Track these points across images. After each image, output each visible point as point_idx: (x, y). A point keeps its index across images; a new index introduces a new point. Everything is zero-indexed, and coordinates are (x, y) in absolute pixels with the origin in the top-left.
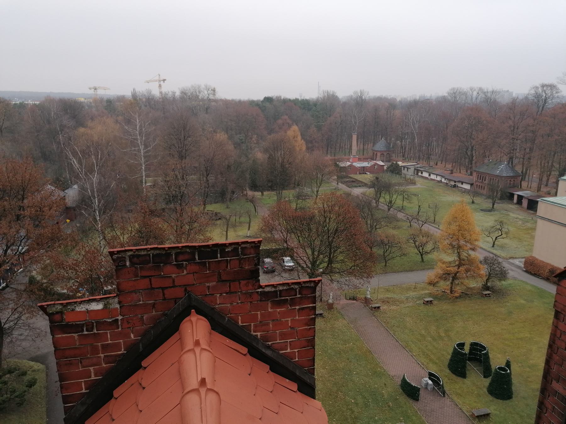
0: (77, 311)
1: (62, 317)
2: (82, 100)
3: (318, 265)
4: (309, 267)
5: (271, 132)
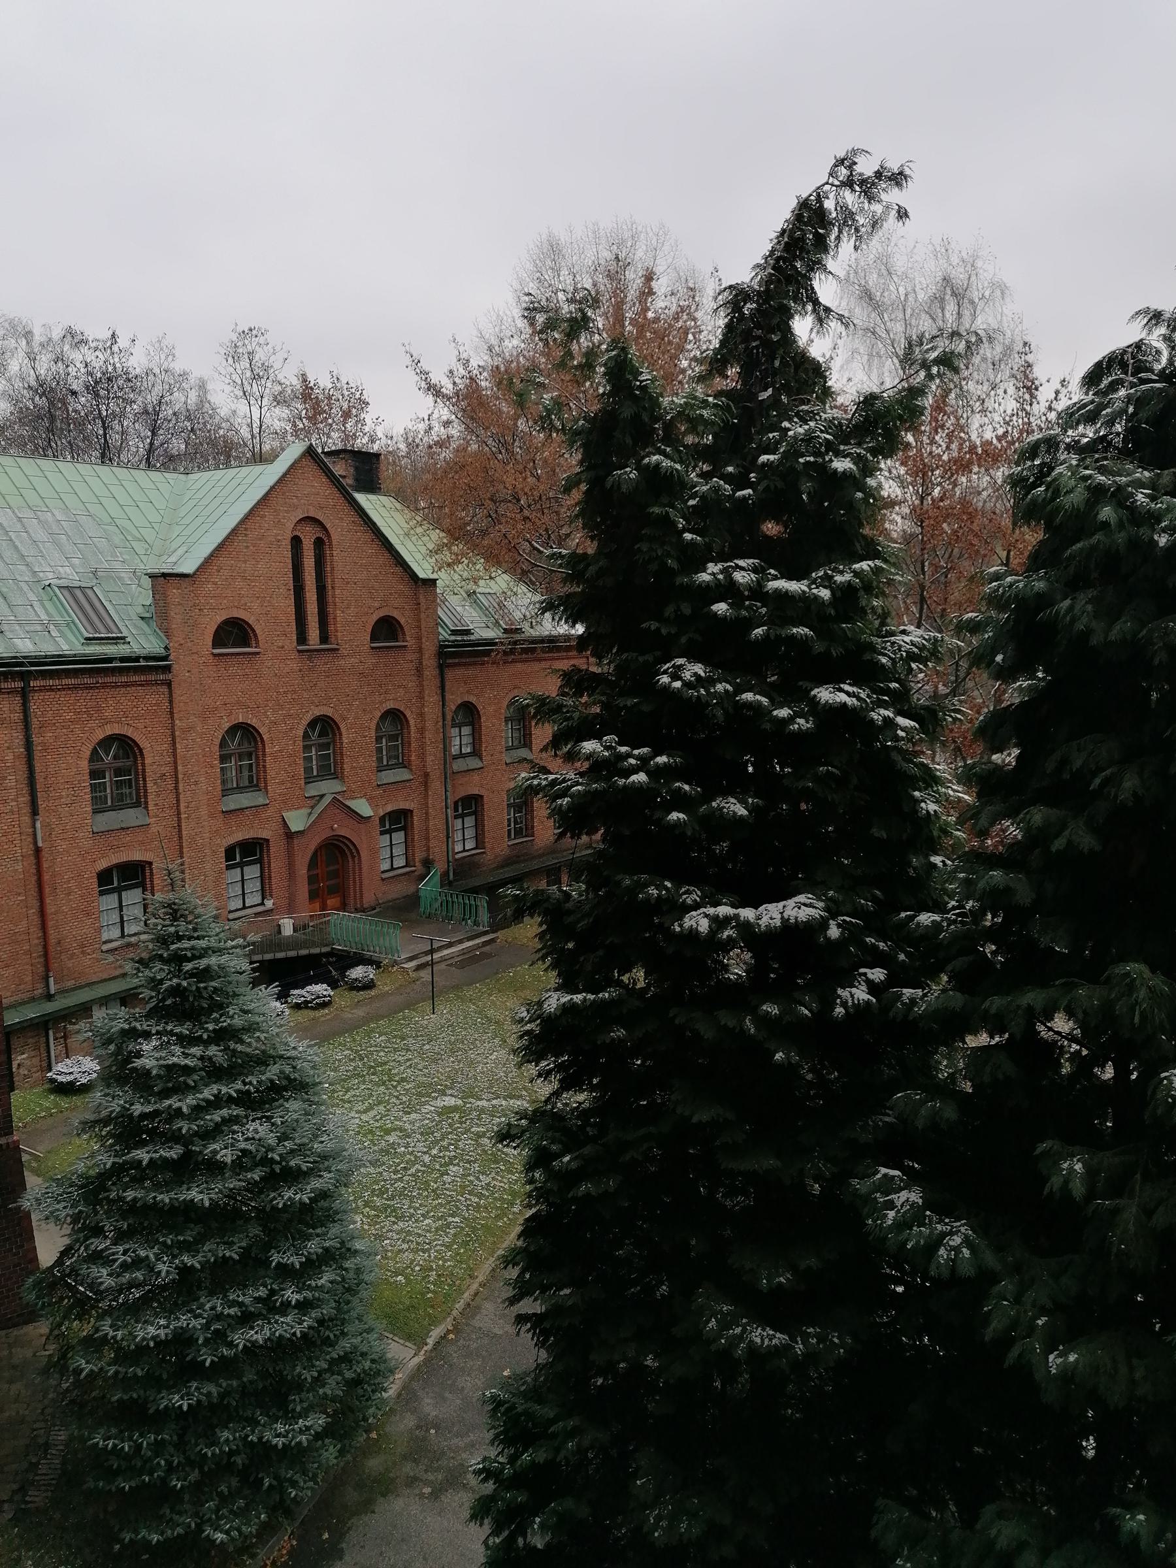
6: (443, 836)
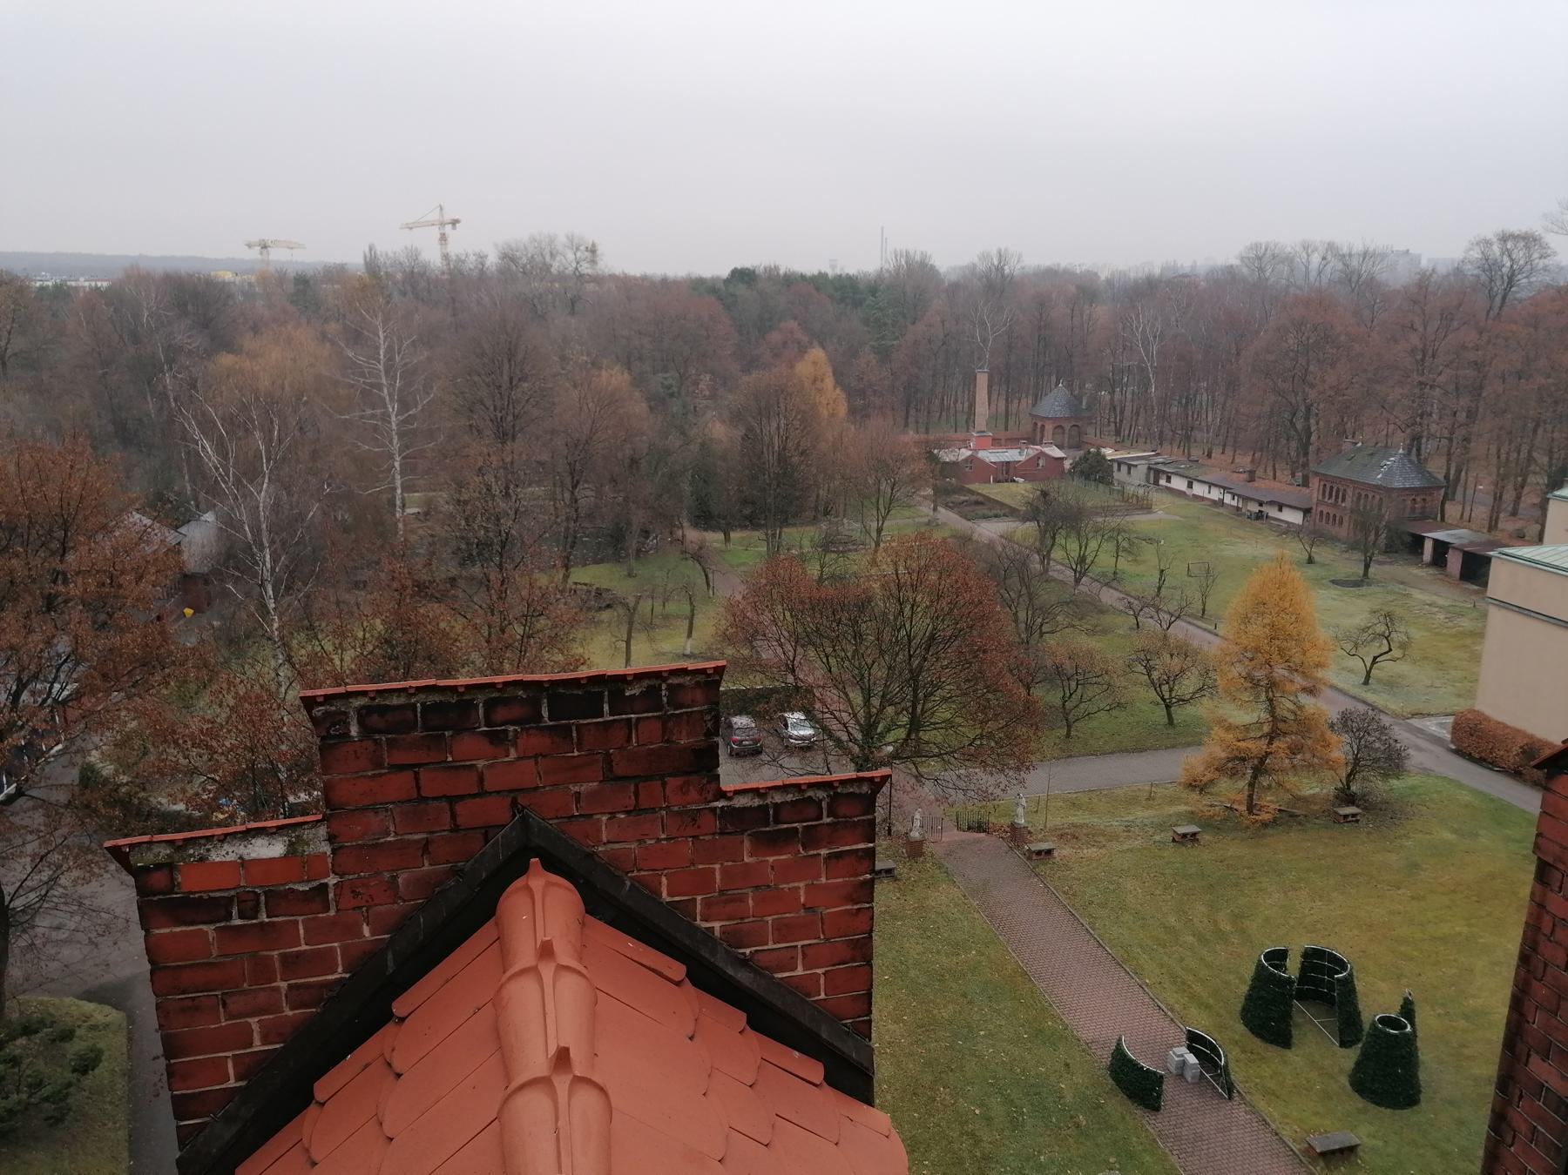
0: (214, 863)
1: (172, 879)
2: (228, 276)
3: (882, 736)
4: (855, 741)
5: (750, 364)
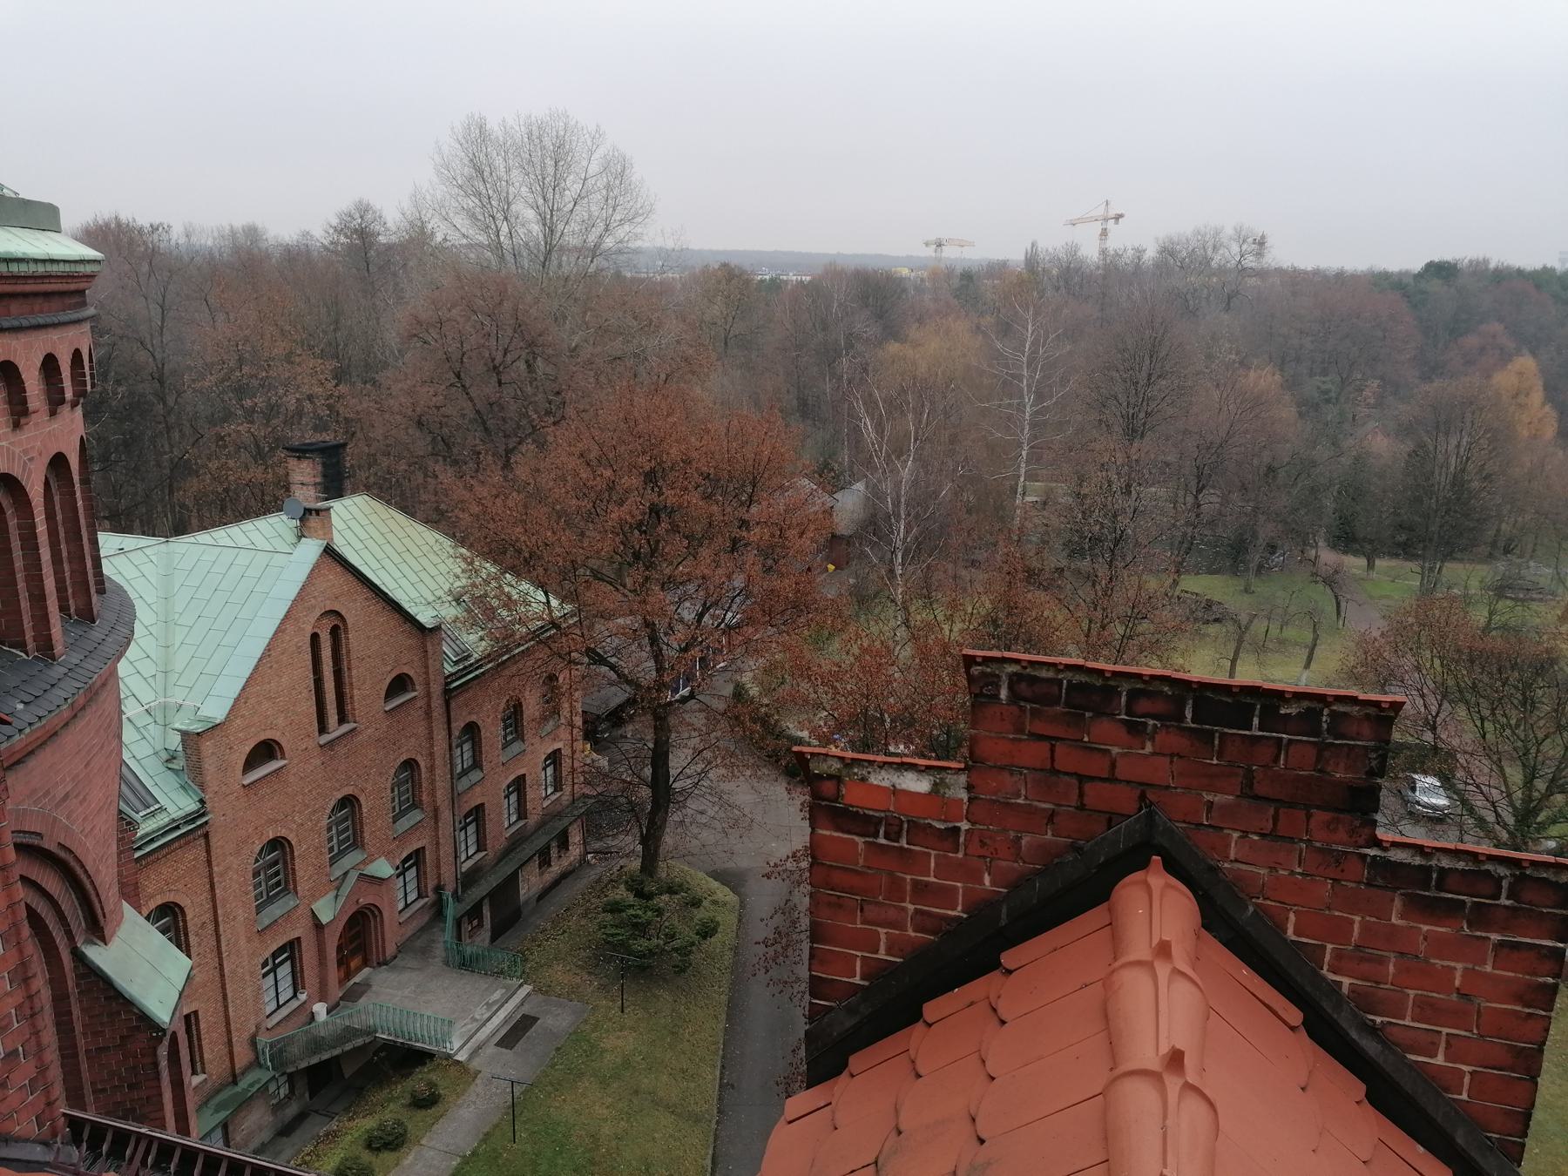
0: (872, 785)
1: (839, 790)
2: (905, 272)
3: (1542, 827)
4: (1505, 826)
5: (1431, 370)
6: (452, 859)
